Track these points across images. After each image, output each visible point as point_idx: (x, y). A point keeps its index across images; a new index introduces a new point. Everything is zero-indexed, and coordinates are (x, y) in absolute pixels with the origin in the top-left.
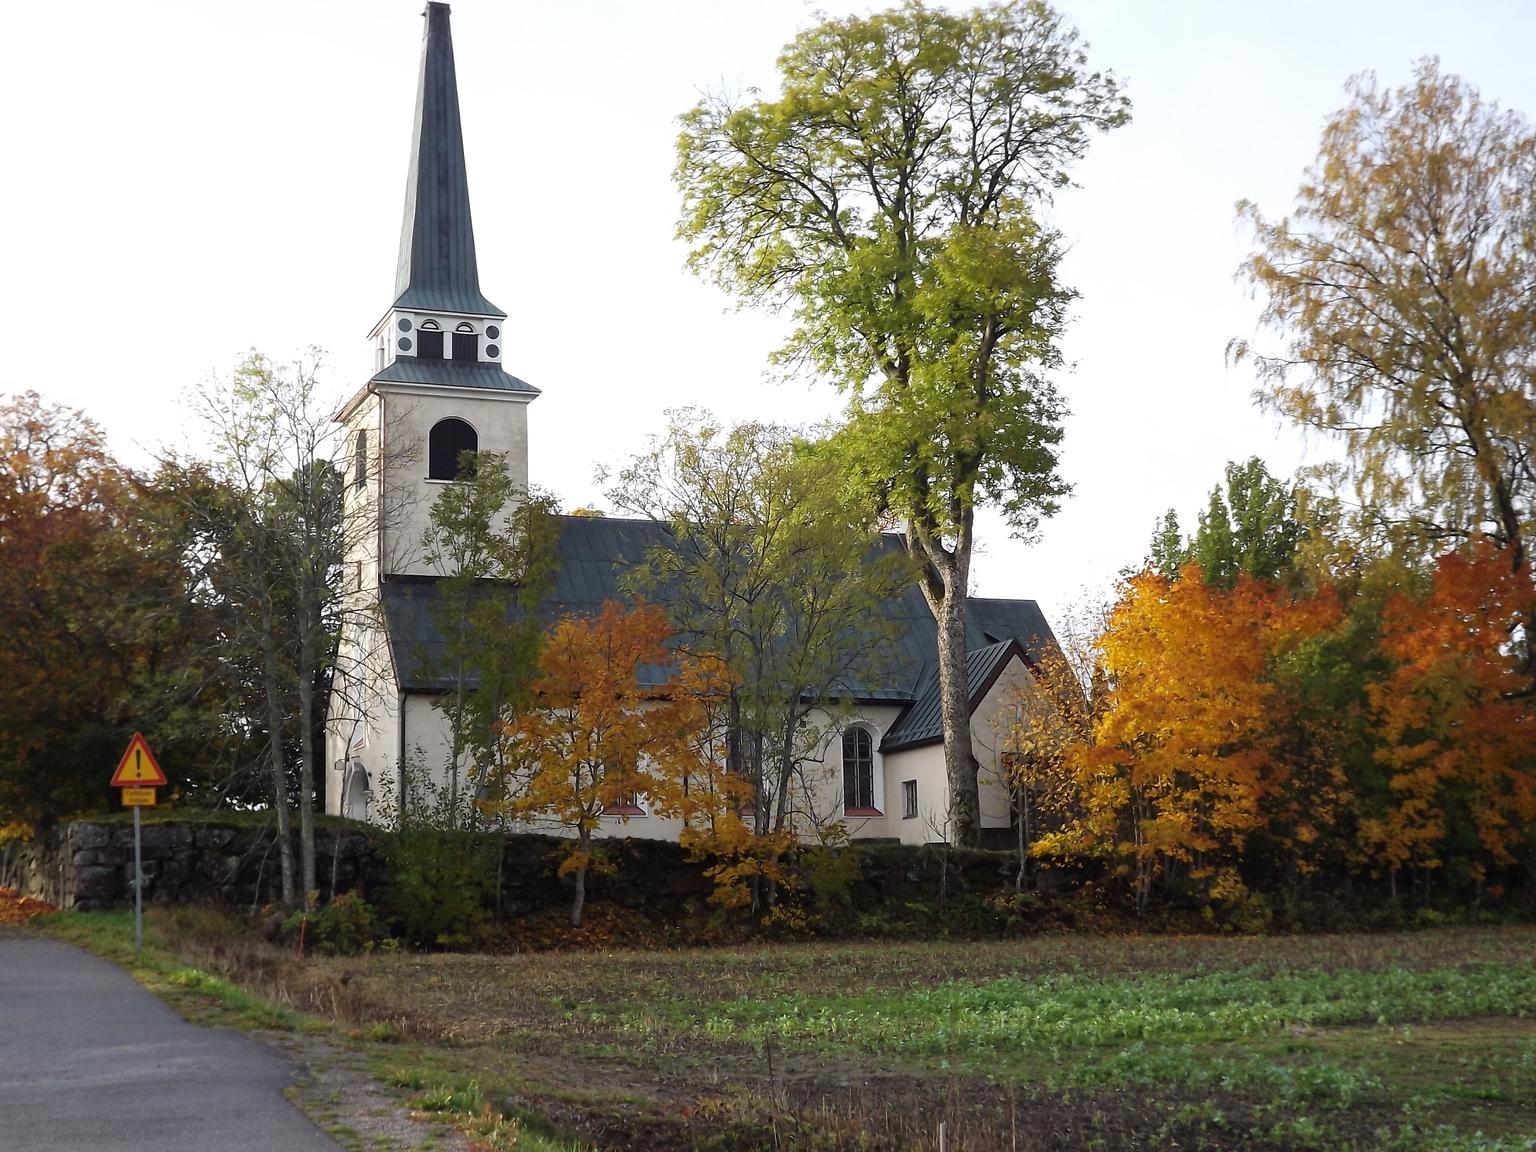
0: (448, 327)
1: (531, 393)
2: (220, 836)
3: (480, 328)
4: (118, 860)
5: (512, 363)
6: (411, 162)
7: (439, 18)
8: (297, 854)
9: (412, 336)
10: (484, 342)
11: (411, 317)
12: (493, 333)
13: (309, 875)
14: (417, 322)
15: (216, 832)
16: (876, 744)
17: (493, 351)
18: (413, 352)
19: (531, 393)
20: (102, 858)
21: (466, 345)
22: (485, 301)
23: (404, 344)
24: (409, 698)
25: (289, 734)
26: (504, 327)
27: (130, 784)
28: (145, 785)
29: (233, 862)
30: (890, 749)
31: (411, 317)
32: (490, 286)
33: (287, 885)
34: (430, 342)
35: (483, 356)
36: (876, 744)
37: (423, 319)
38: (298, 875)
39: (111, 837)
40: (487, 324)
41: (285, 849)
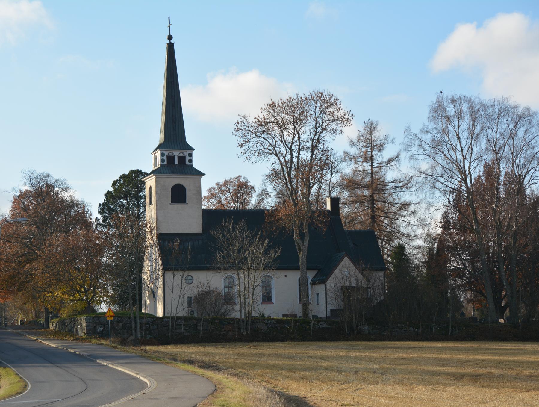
0: (176, 154)
1: (204, 174)
2: (118, 319)
3: (186, 153)
4: (95, 325)
5: (197, 165)
6: (163, 97)
7: (171, 48)
8: (136, 323)
9: (165, 158)
10: (188, 158)
11: (164, 152)
12: (191, 155)
13: (138, 328)
14: (166, 153)
15: (117, 318)
16: (309, 282)
17: (191, 161)
18: (165, 163)
19: (204, 174)
20: (91, 325)
21: (182, 159)
22: (188, 144)
23: (162, 161)
24: (166, 272)
25: (134, 296)
26: (194, 153)
27: (108, 316)
28: (111, 316)
29: (121, 325)
30: (313, 283)
31: (164, 152)
32: (190, 140)
33: (133, 331)
34: (171, 159)
35: (187, 163)
36: (309, 282)
37: (168, 152)
38: (136, 327)
39: (93, 320)
40: (188, 152)
41: (133, 322)
